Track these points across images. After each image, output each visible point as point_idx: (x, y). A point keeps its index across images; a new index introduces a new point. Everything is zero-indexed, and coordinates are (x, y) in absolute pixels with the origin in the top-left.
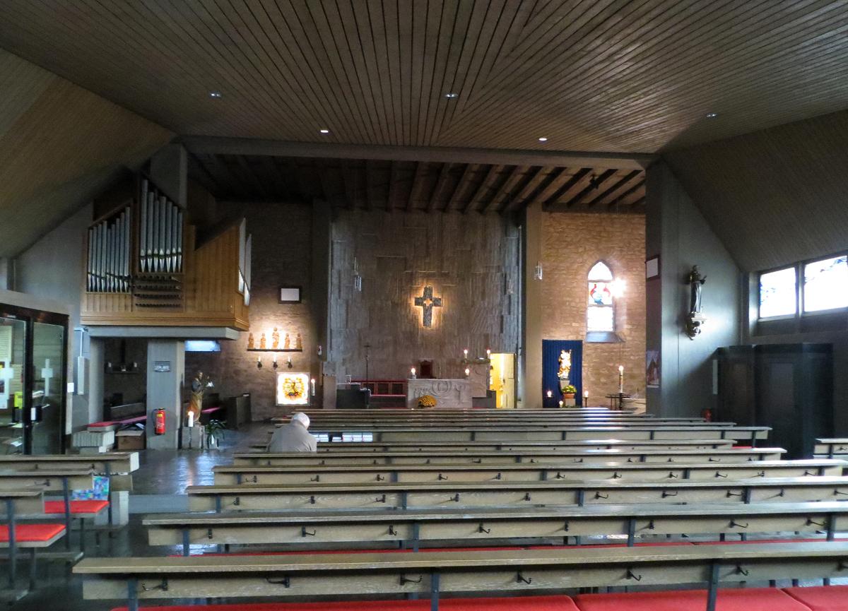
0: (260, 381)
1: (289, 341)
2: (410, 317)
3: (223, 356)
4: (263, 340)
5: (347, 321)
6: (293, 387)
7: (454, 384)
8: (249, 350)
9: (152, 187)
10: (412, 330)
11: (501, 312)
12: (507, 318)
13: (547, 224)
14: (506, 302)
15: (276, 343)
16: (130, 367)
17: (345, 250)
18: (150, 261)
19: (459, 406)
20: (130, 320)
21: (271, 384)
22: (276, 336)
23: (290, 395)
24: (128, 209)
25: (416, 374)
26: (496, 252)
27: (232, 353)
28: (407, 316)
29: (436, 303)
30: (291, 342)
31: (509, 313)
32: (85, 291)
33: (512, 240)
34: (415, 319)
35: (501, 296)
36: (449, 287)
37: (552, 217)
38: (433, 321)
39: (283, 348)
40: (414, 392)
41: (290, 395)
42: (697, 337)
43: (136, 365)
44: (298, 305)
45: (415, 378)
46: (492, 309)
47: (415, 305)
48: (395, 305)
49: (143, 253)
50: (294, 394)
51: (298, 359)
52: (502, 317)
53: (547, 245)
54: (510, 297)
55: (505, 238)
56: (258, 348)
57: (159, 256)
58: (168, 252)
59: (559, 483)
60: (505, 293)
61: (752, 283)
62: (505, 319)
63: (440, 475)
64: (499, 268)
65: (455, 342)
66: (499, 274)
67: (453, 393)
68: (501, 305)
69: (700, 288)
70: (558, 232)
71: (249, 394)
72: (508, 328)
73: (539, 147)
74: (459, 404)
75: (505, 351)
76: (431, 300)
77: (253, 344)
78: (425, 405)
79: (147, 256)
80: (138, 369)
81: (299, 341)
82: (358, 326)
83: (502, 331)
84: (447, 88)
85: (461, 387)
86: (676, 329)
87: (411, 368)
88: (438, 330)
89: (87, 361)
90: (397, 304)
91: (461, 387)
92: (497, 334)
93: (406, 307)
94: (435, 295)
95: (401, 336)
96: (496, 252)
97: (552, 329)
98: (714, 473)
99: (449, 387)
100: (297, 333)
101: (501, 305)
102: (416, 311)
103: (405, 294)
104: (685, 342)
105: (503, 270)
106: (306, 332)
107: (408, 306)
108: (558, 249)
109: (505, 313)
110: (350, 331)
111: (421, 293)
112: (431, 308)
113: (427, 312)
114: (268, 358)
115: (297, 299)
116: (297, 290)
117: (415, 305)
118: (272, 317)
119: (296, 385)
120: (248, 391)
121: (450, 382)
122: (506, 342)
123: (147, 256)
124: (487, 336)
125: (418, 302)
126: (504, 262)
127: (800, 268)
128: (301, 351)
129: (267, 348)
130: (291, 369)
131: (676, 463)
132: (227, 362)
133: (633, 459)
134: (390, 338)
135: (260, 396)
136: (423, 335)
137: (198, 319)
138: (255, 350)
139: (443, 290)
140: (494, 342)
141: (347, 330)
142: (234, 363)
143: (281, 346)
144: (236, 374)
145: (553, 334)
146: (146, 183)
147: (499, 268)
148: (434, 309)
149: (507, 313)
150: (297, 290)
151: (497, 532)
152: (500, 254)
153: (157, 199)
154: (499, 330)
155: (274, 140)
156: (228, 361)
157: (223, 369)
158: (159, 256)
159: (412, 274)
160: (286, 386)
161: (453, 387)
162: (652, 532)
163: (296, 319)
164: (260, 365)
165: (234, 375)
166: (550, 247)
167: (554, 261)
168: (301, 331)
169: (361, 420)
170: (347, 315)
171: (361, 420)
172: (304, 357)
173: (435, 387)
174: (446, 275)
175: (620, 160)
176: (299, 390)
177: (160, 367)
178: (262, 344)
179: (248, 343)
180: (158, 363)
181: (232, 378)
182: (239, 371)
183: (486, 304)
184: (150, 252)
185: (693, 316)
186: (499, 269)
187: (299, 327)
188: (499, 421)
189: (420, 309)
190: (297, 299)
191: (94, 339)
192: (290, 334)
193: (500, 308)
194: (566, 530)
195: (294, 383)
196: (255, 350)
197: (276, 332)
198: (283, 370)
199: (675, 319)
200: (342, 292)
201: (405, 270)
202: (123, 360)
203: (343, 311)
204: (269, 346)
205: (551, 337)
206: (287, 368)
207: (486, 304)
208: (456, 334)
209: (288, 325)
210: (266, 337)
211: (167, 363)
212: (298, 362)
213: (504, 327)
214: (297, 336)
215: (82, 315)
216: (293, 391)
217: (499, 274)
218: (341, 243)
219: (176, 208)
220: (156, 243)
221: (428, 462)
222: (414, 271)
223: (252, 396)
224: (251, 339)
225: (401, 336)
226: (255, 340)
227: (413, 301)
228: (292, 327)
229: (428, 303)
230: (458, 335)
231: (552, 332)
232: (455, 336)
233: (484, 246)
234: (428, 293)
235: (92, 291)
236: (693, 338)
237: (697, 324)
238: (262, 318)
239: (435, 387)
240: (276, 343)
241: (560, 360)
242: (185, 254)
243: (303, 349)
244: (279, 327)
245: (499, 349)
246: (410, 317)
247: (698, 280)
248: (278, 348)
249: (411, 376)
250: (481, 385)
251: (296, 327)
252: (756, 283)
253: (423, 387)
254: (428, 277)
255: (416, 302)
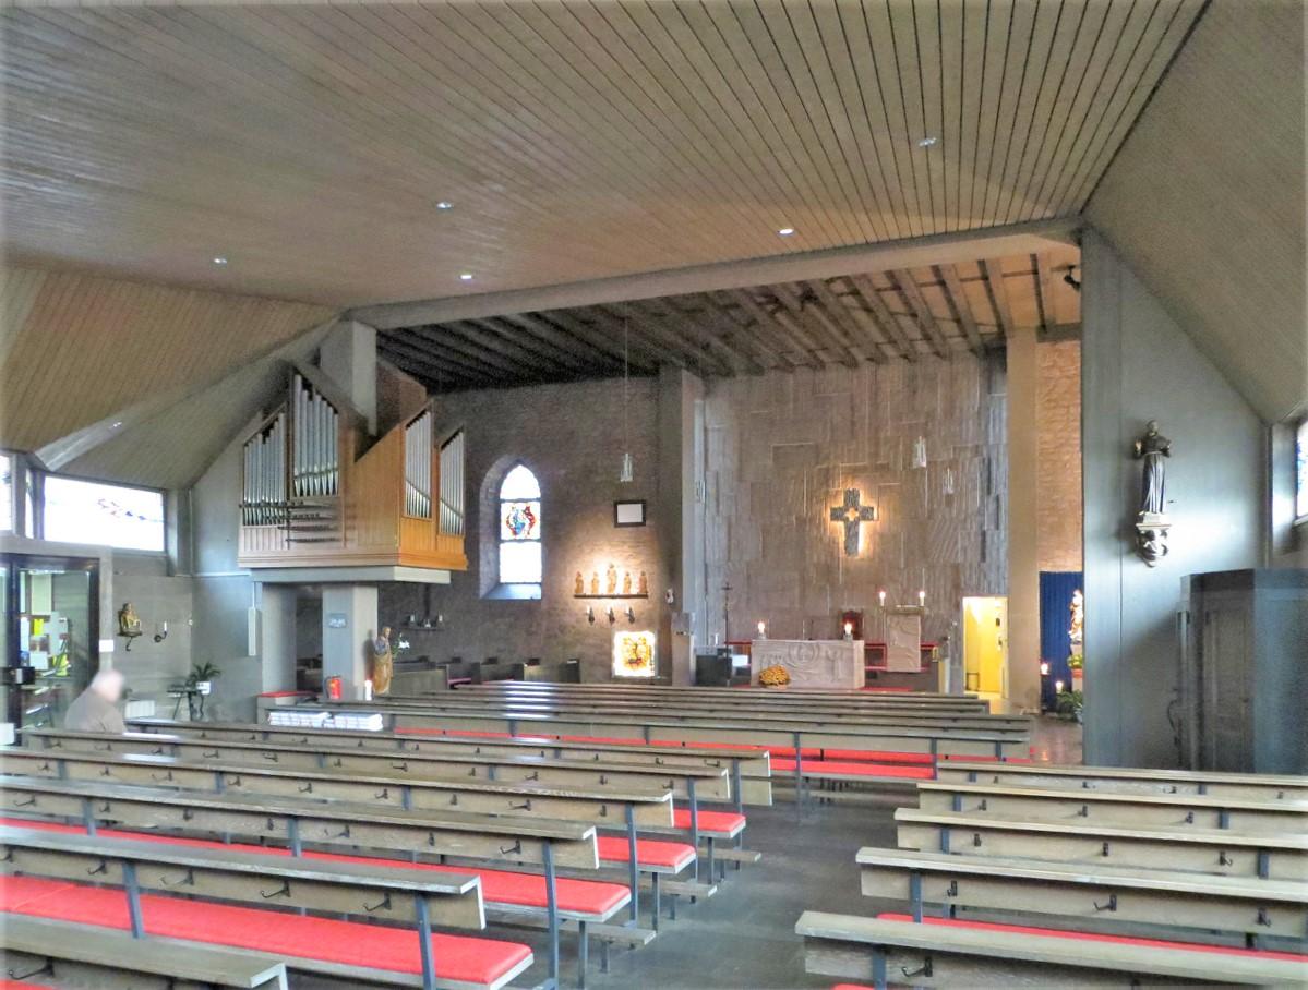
0: (591, 641)
1: (630, 583)
2: (826, 540)
3: (544, 607)
4: (594, 582)
5: (729, 552)
6: (635, 650)
7: (824, 647)
8: (577, 597)
9: (307, 385)
10: (829, 562)
11: (982, 525)
12: (992, 536)
13: (1046, 365)
14: (992, 507)
15: (612, 586)
16: (434, 623)
17: (725, 441)
18: (331, 476)
19: (832, 685)
20: (269, 561)
21: (607, 646)
22: (611, 574)
23: (631, 662)
24: (282, 416)
25: (765, 631)
26: (971, 422)
27: (556, 602)
28: (821, 539)
29: (866, 514)
30: (633, 584)
31: (997, 527)
32: (242, 527)
33: (1000, 399)
34: (833, 542)
35: (982, 498)
36: (890, 487)
37: (1056, 351)
38: (863, 545)
39: (621, 593)
40: (761, 661)
41: (631, 662)
42: (1160, 561)
43: (441, 619)
44: (641, 528)
45: (764, 637)
46: (965, 520)
47: (832, 519)
48: (802, 522)
49: (296, 473)
50: (636, 662)
51: (641, 610)
52: (984, 534)
53: (1049, 401)
54: (997, 499)
55: (989, 397)
56: (589, 593)
57: (314, 475)
58: (323, 469)
59: (338, 773)
60: (989, 493)
61: (1279, 446)
62: (988, 538)
63: (602, 778)
64: (977, 450)
65: (900, 579)
66: (976, 460)
67: (823, 663)
68: (980, 513)
69: (1160, 466)
70: (1068, 377)
71: (578, 660)
72: (994, 553)
73: (458, 291)
74: (832, 681)
75: (999, 594)
76: (857, 510)
77: (582, 588)
78: (766, 681)
79: (301, 475)
80: (443, 625)
81: (643, 582)
82: (747, 558)
83: (983, 557)
84: (915, 132)
85: (835, 653)
86: (1115, 545)
87: (758, 622)
88: (871, 559)
89: (259, 614)
90: (805, 521)
91: (835, 653)
92: (975, 565)
93: (820, 523)
94: (863, 501)
95: (812, 573)
96: (971, 422)
97: (1057, 552)
98: (597, 777)
99: (816, 654)
100: (640, 571)
101: (980, 513)
102: (834, 531)
103: (817, 503)
104: (1134, 570)
105: (985, 453)
106: (653, 570)
107: (822, 521)
108: (1068, 407)
109: (988, 526)
110: (734, 565)
111: (840, 503)
112: (842, 520)
113: (852, 530)
114: (602, 608)
115: (640, 520)
116: (640, 506)
117: (832, 519)
118: (607, 549)
119: (639, 647)
120: (577, 657)
121: (818, 645)
122: (992, 576)
123: (301, 475)
124: (956, 568)
125: (837, 515)
126: (987, 437)
127: (38, 477)
128: (645, 596)
129: (600, 593)
130: (634, 625)
131: (425, 752)
132: (550, 615)
133: (547, 752)
134: (796, 575)
135: (592, 664)
136: (847, 571)
137: (365, 556)
138: (585, 597)
139: (879, 493)
140: (970, 579)
141: (730, 564)
142: (558, 615)
143: (619, 590)
144: (562, 632)
145: (1059, 562)
146: (299, 379)
147: (977, 450)
148: (863, 527)
149: (992, 527)
150: (640, 506)
151: (362, 838)
152: (979, 425)
153: (311, 398)
154: (979, 557)
155: (380, 305)
156: (549, 614)
157: (545, 623)
158: (314, 475)
159: (828, 470)
160: (625, 649)
161: (823, 654)
162: (515, 857)
163: (638, 549)
164: (591, 619)
165: (559, 634)
166: (1052, 404)
167: (1061, 430)
168: (646, 568)
169: (463, 698)
170: (729, 540)
171: (463, 698)
172: (651, 606)
173: (794, 652)
174: (885, 468)
175: (1015, 237)
176: (642, 656)
177: (335, 621)
178: (594, 589)
179: (575, 586)
180: (334, 616)
181: (556, 636)
182: (565, 627)
183: (955, 512)
184: (304, 470)
185: (1141, 519)
186: (977, 452)
187: (643, 562)
188: (572, 692)
189: (840, 525)
190: (640, 520)
191: (268, 586)
192: (630, 571)
193: (978, 518)
194: (955, 894)
195: (636, 646)
196: (585, 597)
197: (611, 570)
198: (622, 627)
199: (1113, 528)
200: (721, 507)
201: (817, 464)
202: (302, 606)
203: (723, 535)
204: (603, 590)
205: (1054, 566)
206: (628, 623)
207: (955, 512)
208: (902, 566)
209: (627, 559)
210: (599, 578)
211: (343, 616)
212: (642, 613)
213: (987, 551)
214: (639, 575)
215: (240, 555)
216: (634, 657)
217: (976, 460)
218: (719, 430)
219: (331, 409)
220: (311, 461)
221: (360, 745)
222: (831, 466)
223: (581, 664)
224: (579, 582)
225: (812, 573)
226: (585, 582)
227: (827, 514)
228: (633, 562)
229: (851, 515)
230: (907, 565)
231: (1059, 557)
232: (899, 569)
233: (950, 412)
234: (852, 498)
235: (253, 524)
236: (1151, 563)
237: (1150, 536)
238: (593, 550)
239: (794, 652)
240: (612, 586)
241: (1072, 607)
242: (344, 469)
243: (649, 594)
244: (616, 562)
245: (978, 589)
246: (826, 540)
247: (1154, 448)
248: (615, 593)
249: (757, 634)
250: (909, 650)
251: (638, 562)
252: (1288, 445)
253: (774, 653)
254: (854, 473)
255: (832, 515)
